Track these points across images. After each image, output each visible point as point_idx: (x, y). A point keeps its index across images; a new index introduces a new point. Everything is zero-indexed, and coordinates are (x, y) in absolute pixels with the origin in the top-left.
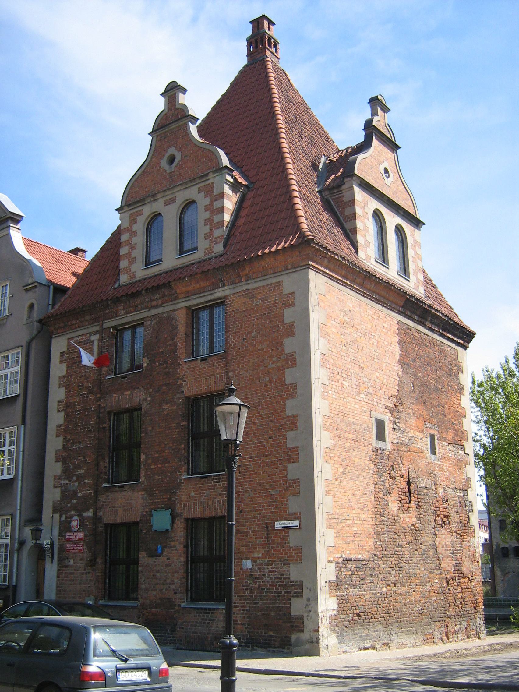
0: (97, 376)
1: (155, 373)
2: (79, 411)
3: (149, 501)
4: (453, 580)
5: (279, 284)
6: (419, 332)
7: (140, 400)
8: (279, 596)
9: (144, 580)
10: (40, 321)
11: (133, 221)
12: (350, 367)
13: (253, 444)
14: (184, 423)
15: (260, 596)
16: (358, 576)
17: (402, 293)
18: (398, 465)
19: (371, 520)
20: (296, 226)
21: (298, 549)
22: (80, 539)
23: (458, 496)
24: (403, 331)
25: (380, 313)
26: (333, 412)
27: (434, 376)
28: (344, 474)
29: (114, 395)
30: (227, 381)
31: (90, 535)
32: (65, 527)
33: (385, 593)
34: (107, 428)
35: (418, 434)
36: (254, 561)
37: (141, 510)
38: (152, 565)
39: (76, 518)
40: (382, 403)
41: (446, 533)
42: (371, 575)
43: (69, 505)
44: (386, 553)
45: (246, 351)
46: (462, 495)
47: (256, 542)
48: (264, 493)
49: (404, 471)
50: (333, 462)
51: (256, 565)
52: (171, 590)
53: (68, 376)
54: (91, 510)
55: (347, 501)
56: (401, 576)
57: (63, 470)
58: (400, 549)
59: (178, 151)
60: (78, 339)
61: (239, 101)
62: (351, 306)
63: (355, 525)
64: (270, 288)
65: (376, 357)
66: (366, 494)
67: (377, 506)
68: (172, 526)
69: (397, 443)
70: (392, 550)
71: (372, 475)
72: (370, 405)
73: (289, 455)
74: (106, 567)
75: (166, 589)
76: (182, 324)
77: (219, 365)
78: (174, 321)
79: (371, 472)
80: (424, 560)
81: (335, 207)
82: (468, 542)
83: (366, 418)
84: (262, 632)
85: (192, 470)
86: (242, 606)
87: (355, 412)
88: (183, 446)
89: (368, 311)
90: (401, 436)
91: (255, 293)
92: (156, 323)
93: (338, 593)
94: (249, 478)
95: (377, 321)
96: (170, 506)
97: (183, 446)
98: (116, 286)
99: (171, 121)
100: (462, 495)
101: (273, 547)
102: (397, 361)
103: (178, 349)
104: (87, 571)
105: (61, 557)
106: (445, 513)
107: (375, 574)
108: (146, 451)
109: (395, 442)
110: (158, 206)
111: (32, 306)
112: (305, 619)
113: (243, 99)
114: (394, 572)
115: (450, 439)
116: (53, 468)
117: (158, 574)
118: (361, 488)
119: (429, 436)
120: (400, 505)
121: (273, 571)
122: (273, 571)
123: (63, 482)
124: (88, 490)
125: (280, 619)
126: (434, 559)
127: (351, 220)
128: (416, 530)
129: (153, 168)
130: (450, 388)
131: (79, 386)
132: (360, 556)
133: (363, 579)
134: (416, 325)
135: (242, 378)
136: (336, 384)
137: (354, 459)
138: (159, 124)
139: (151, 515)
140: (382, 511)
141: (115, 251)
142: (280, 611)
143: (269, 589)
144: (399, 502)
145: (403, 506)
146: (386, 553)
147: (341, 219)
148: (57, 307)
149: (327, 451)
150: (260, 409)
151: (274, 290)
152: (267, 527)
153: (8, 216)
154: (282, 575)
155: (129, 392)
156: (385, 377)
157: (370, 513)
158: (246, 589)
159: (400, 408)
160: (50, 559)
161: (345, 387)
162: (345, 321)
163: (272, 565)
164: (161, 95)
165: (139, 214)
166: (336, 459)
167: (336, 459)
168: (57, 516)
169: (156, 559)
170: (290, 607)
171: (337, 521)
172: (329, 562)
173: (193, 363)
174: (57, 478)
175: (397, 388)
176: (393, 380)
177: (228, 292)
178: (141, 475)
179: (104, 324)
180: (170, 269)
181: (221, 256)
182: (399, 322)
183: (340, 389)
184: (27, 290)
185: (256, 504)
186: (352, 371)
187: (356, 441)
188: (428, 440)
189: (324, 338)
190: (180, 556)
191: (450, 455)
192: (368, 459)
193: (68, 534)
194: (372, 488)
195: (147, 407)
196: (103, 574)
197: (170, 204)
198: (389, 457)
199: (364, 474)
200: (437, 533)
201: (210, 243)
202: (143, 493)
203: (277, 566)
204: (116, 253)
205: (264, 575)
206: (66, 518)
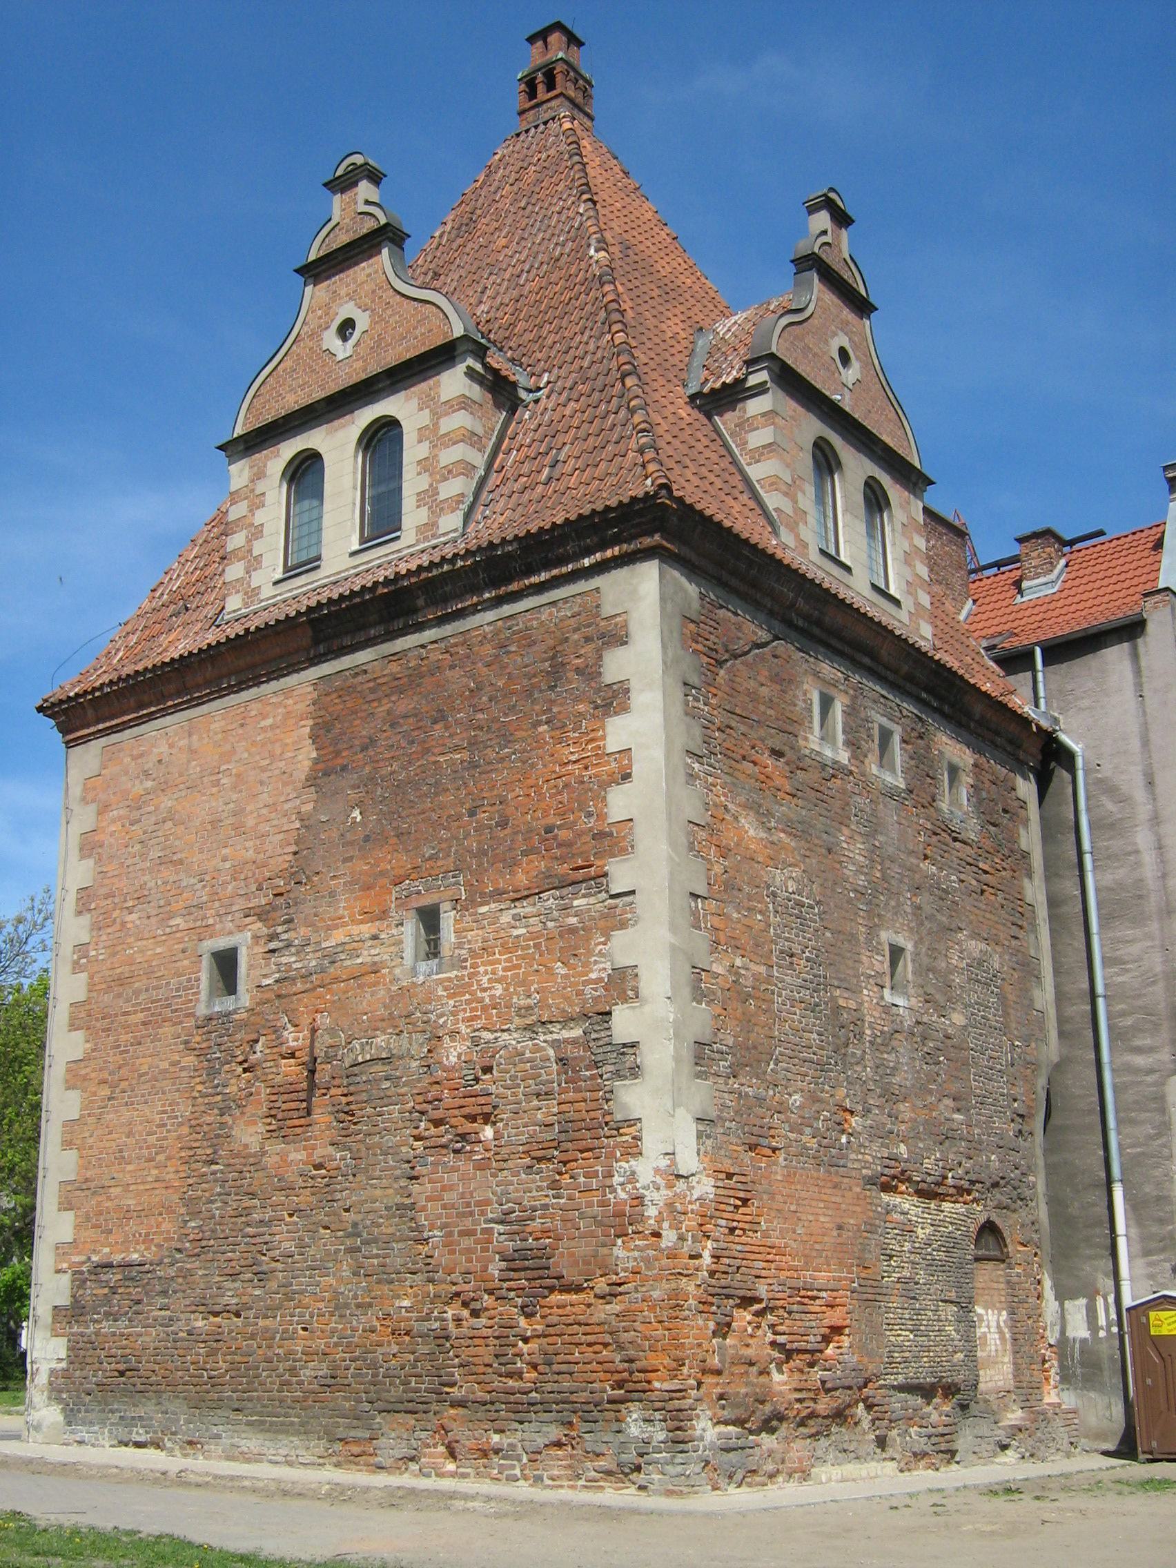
17: (281, 627)
80: (352, 1250)
132: (135, 1256)
133: (138, 1302)
172: (58, 1271)
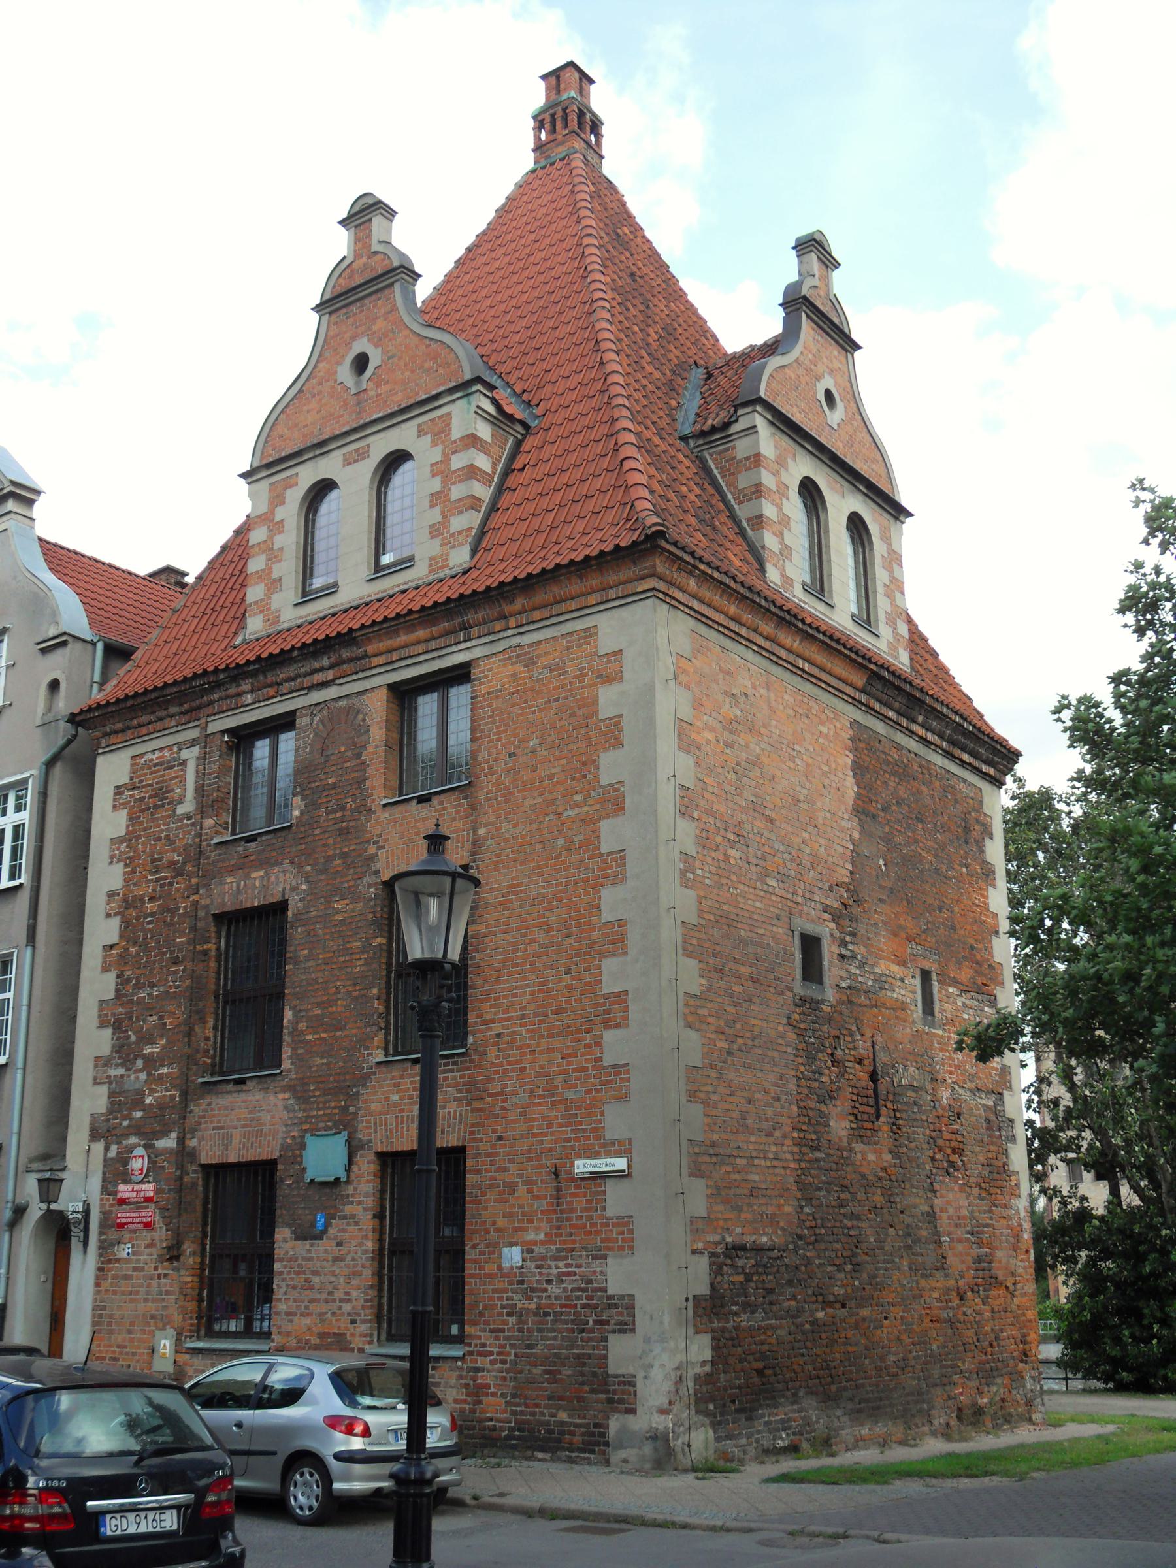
0: (193, 840)
1: (317, 831)
2: (152, 915)
3: (300, 1114)
4: (972, 1290)
5: (589, 634)
6: (899, 747)
7: (284, 889)
8: (582, 1331)
9: (285, 1293)
10: (73, 719)
11: (277, 499)
12: (744, 817)
13: (527, 986)
14: (379, 940)
15: (540, 1330)
16: (760, 1286)
18: (851, 1035)
19: (788, 1156)
20: (629, 506)
21: (626, 1224)
22: (148, 1200)
23: (984, 1105)
24: (862, 742)
25: (812, 703)
26: (706, 916)
27: (930, 843)
28: (729, 1053)
29: (229, 880)
30: (474, 846)
31: (170, 1190)
32: (116, 1172)
33: (821, 1323)
34: (213, 953)
35: (894, 968)
36: (528, 1251)
37: (281, 1135)
38: (304, 1259)
39: (140, 1151)
40: (816, 898)
41: (956, 1189)
42: (790, 1283)
43: (125, 1123)
44: (823, 1231)
45: (515, 780)
46: (991, 1103)
47: (532, 1205)
48: (550, 1096)
49: (863, 1048)
50: (704, 1027)
51: (532, 1259)
52: (342, 1314)
53: (130, 838)
54: (174, 1135)
55: (736, 1115)
56: (857, 1283)
57: (113, 1046)
58: (855, 1223)
59: (376, 346)
60: (154, 757)
61: (513, 245)
62: (748, 683)
63: (754, 1169)
64: (569, 642)
65: (801, 798)
66: (778, 1099)
67: (804, 1127)
68: (348, 1169)
69: (850, 987)
70: (838, 1224)
71: (792, 1057)
72: (790, 904)
73: (607, 1012)
74: (202, 1263)
75: (333, 1314)
76: (378, 723)
77: (457, 813)
78: (360, 717)
79: (790, 1050)
81: (716, 472)
82: (1006, 1206)
83: (780, 930)
84: (543, 1414)
85: (395, 1046)
86: (499, 1354)
87: (756, 917)
88: (375, 991)
89: (786, 697)
90: (858, 972)
91: (538, 652)
92: (322, 721)
93: (716, 1325)
94: (517, 1062)
95: (806, 721)
96: (345, 1123)
97: (375, 991)
98: (238, 641)
99: (365, 285)
100: (991, 1103)
101: (568, 1219)
102: (850, 808)
103: (367, 778)
104: (160, 1271)
105: (105, 1240)
106: (954, 1144)
107: (799, 1281)
108: (296, 1002)
109: (844, 985)
110: (328, 466)
111: (54, 685)
112: (639, 1386)
113: (523, 241)
114: (842, 1275)
115: (965, 981)
116: (93, 1040)
117: (316, 1280)
118: (767, 1085)
119: (918, 973)
120: (854, 1126)
121: (569, 1274)
122: (569, 1274)
123: (114, 1072)
124: (167, 1090)
125: (583, 1383)
126: (931, 1246)
127: (751, 499)
128: (891, 1180)
129: (321, 384)
130: (964, 870)
131: (154, 860)
133: (771, 1291)
134: (891, 731)
135: (506, 840)
136: (714, 854)
137: (754, 1021)
138: (334, 287)
139: (303, 1146)
140: (814, 1137)
141: (239, 567)
142: (584, 1365)
143: (561, 1313)
144: (852, 1118)
145: (863, 1130)
146: (823, 1231)
147: (730, 496)
148: (109, 687)
149: (691, 1002)
150: (545, 910)
151: (579, 646)
152: (556, 1174)
153: (5, 491)
154: (590, 1282)
155: (262, 873)
156: (822, 841)
157: (788, 1142)
158: (509, 1314)
159: (856, 910)
160: (81, 1244)
161: (733, 861)
162: (736, 716)
163: (566, 1258)
164: (340, 223)
165: (289, 484)
166: (710, 1020)
167: (710, 1020)
168: (99, 1147)
169: (311, 1245)
170: (605, 1357)
171: (714, 1159)
172: (694, 1252)
173: (400, 808)
174: (102, 1062)
175: (849, 867)
176: (840, 849)
177: (477, 653)
178: (284, 1056)
179: (210, 725)
180: (355, 603)
181: (465, 572)
182: (855, 724)
183: (722, 864)
184: (44, 651)
185: (536, 1120)
186: (748, 827)
187: (757, 981)
188: (918, 982)
189: (688, 752)
190: (366, 1237)
191: (966, 1016)
192: (785, 1021)
193: (122, 1188)
194: (792, 1086)
195: (299, 904)
196: (196, 1279)
197: (357, 461)
198: (830, 1019)
199: (776, 1054)
200: (937, 1186)
201: (442, 545)
202: (287, 1095)
203: (580, 1261)
204: (241, 572)
205: (549, 1282)
206: (118, 1153)
